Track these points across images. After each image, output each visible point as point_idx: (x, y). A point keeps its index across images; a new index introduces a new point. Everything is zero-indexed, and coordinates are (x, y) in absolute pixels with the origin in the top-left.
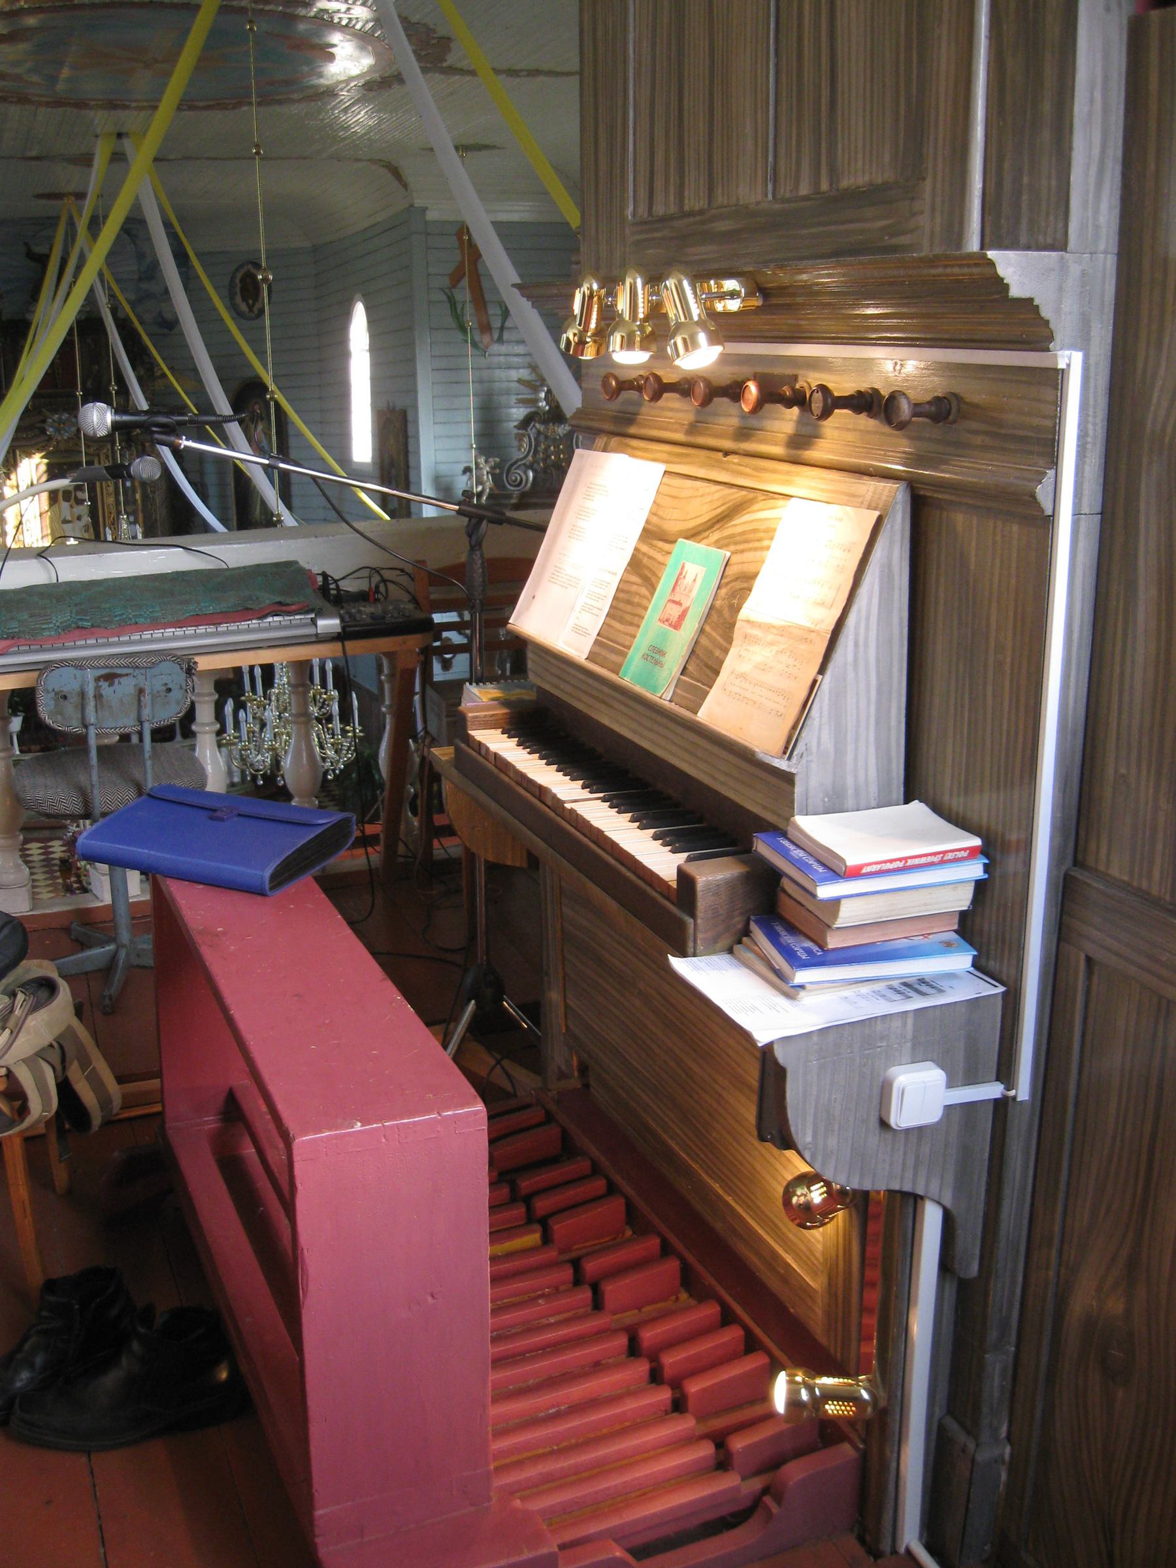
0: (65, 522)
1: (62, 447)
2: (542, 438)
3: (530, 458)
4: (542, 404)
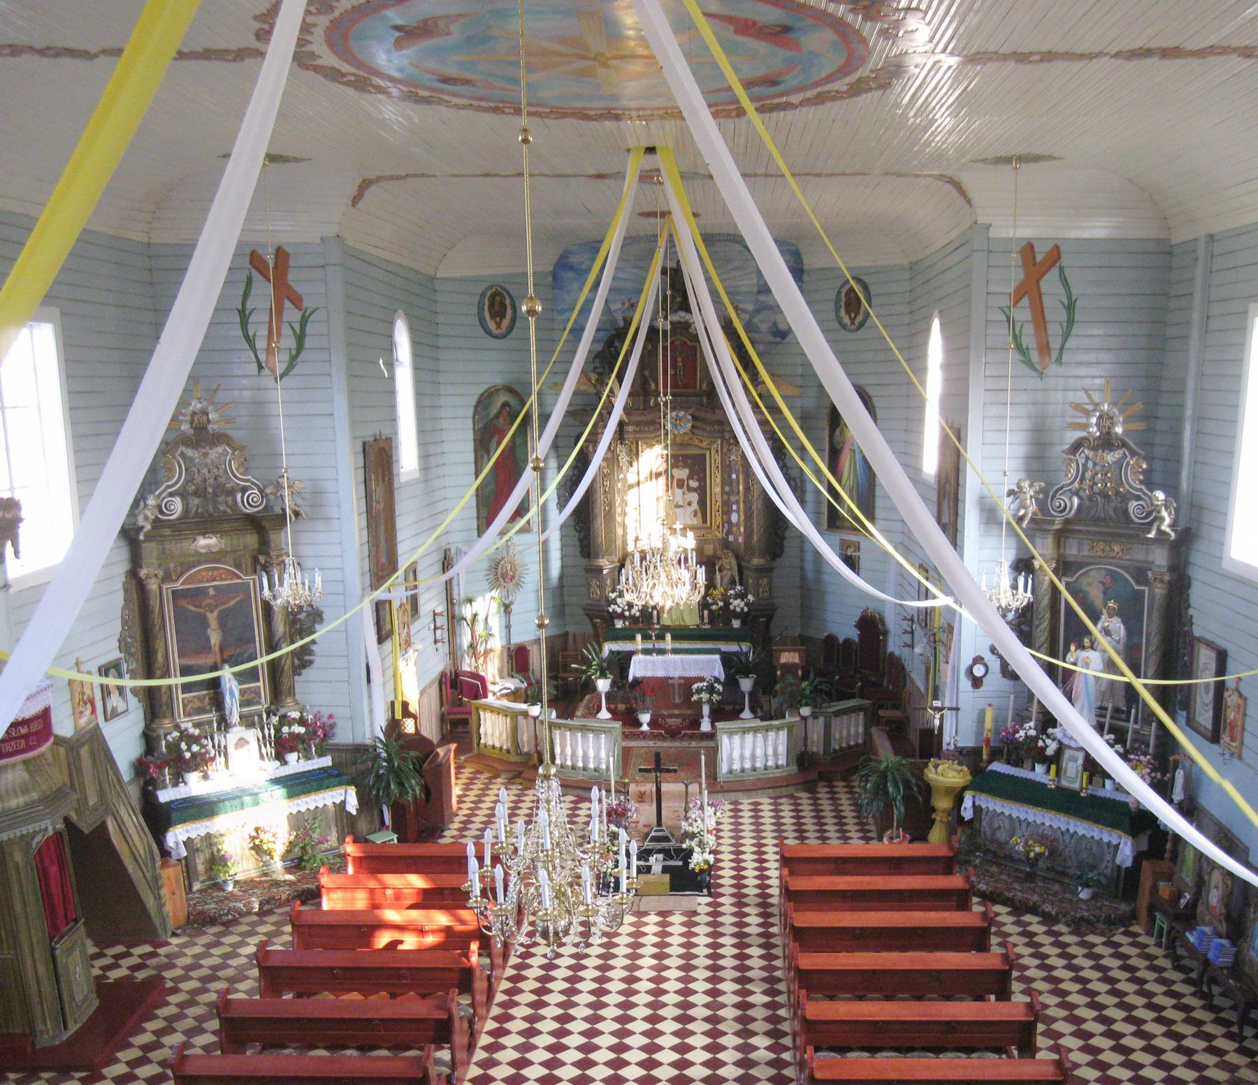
0: (678, 506)
1: (678, 440)
2: (1090, 464)
3: (1076, 484)
4: (1094, 429)
